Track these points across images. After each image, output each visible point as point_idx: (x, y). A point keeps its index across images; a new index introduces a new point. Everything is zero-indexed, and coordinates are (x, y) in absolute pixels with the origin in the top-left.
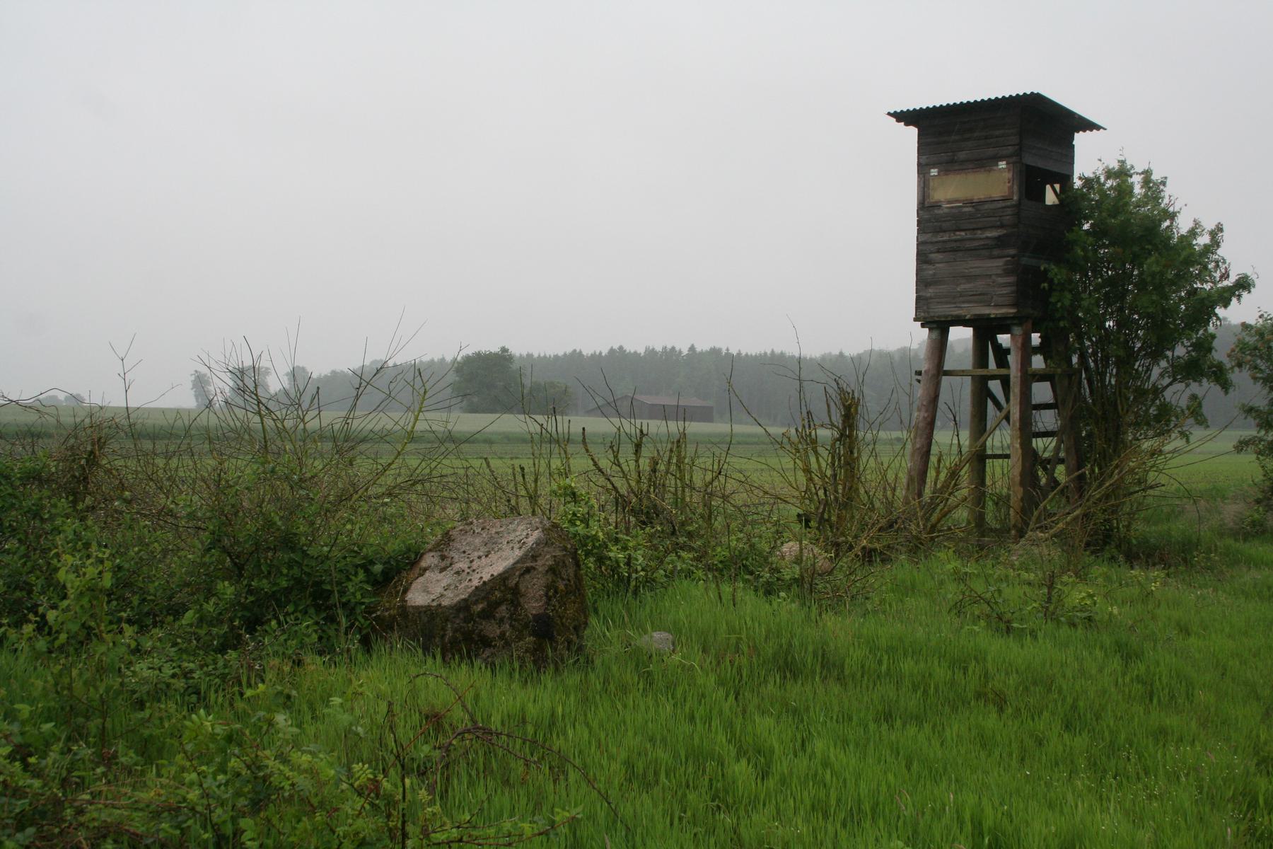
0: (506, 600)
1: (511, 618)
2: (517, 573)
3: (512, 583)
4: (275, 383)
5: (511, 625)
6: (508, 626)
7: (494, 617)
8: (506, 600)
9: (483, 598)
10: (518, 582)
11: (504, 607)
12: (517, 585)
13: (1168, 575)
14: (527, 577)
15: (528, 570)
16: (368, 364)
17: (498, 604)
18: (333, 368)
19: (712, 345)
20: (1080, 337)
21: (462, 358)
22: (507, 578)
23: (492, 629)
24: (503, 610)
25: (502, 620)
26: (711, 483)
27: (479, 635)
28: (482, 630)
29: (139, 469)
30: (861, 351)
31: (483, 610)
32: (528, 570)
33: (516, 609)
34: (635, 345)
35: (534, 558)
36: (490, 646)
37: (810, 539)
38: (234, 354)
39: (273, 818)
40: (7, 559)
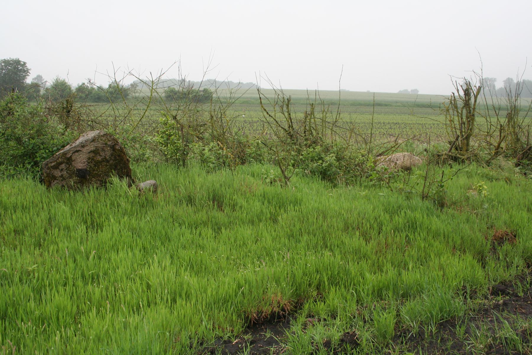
0: (64, 162)
1: (66, 169)
2: (71, 152)
3: (68, 156)
5: (67, 172)
6: (65, 172)
7: (58, 168)
8: (64, 162)
9: (55, 161)
10: (71, 156)
11: (64, 165)
12: (71, 156)
14: (77, 154)
15: (77, 151)
16: (206, 81)
17: (61, 163)
20: (76, 109)
21: (173, 88)
24: (63, 166)
25: (62, 170)
27: (52, 175)
28: (52, 173)
29: (131, 118)
32: (77, 151)
33: (69, 166)
34: (245, 81)
36: (56, 179)
37: (443, 155)
40: (1, 160)
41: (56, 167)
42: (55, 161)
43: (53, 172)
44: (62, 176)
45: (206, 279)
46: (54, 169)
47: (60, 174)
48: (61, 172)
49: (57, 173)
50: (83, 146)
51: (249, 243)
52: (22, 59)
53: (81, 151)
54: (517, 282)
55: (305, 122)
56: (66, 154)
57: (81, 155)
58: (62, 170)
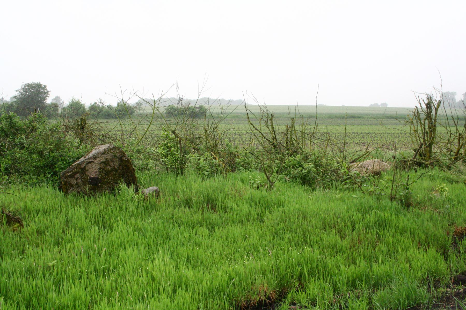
4: (127, 105)
5: (81, 181)
6: (80, 181)
7: (74, 177)
9: (71, 171)
11: (79, 174)
13: (176, 160)
14: (90, 165)
15: (90, 162)
17: (77, 173)
18: (77, 98)
19: (383, 102)
22: (81, 165)
23: (73, 181)
25: (77, 178)
26: (196, 139)
30: (192, 99)
31: (71, 175)
32: (90, 162)
35: (95, 158)
38: (453, 104)
39: (192, 273)
41: (72, 176)
43: (69, 180)
47: (75, 182)
56: (81, 165)
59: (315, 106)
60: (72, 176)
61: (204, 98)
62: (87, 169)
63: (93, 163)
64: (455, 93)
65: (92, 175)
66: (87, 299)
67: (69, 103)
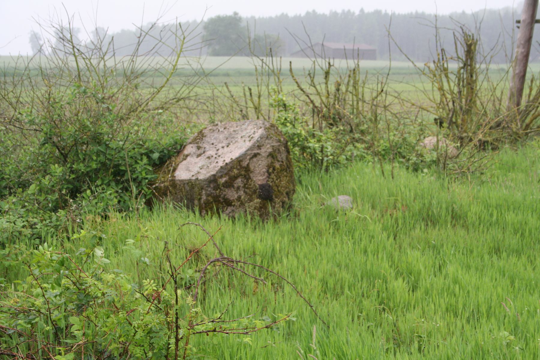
0: (241, 175)
2: (248, 157)
3: (245, 164)
5: (244, 192)
6: (242, 192)
7: (233, 186)
9: (226, 174)
12: (248, 165)
14: (255, 159)
15: (255, 155)
17: (236, 178)
24: (239, 182)
25: (238, 188)
28: (225, 195)
32: (255, 155)
41: (229, 185)
42: (226, 174)
43: (224, 193)
44: (239, 198)
45: (313, 285)
46: (227, 187)
47: (236, 196)
48: (237, 193)
49: (232, 195)
50: (259, 147)
51: (364, 239)
52: (227, 12)
53: (259, 154)
54: (329, 166)
55: (139, 37)
56: (241, 161)
57: (260, 162)
58: (238, 188)
59: (363, 59)
60: (229, 185)
61: (123, 31)
62: (252, 167)
63: (259, 157)
64: (97, 31)
65: (259, 180)
66: (80, 64)
67: (300, 15)
